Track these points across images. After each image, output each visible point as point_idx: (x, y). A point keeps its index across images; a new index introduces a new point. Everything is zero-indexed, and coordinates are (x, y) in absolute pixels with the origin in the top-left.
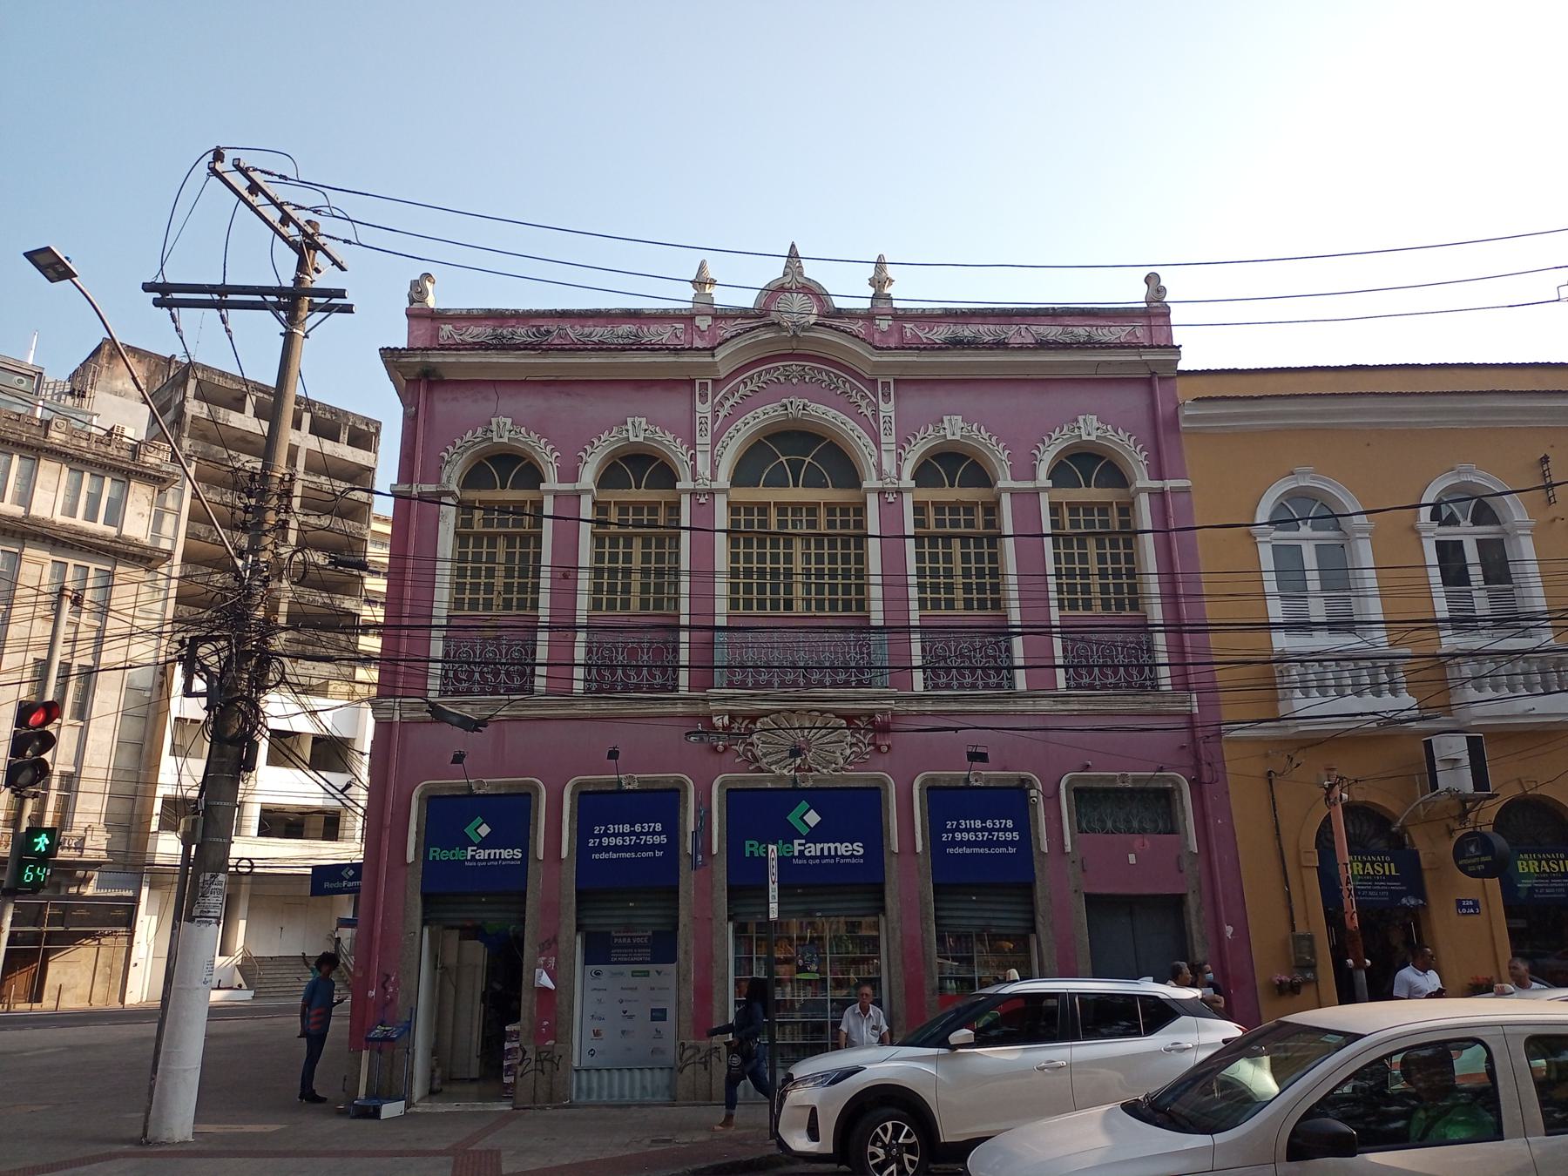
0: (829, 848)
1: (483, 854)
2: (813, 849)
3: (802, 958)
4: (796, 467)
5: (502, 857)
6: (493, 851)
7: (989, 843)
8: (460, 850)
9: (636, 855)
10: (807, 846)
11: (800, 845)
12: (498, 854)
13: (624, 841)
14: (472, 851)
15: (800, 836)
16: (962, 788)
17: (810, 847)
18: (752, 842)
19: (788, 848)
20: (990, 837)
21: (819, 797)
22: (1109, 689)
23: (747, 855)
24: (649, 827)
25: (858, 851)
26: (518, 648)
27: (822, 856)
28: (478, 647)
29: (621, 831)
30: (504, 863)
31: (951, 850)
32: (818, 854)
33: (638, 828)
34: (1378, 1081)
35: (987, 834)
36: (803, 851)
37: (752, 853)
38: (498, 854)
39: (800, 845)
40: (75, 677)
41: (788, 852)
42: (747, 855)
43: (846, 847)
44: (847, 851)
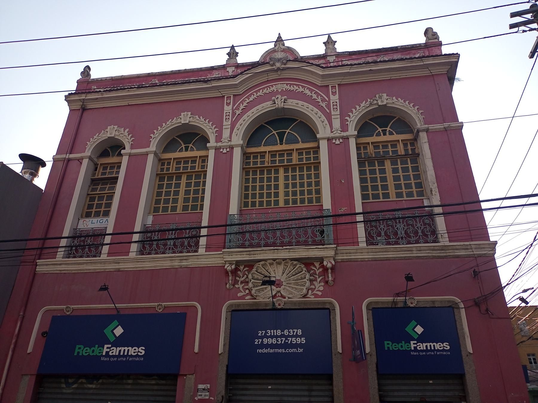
0: (276, 350)
1: (115, 351)
4: (281, 135)
5: (130, 354)
6: (123, 349)
7: (286, 346)
10: (418, 344)
11: (414, 344)
12: (294, 351)
13: (277, 341)
14: (107, 348)
15: (414, 340)
17: (420, 345)
19: (408, 345)
20: (287, 341)
23: (386, 349)
24: (294, 332)
25: (447, 347)
27: (119, 356)
29: (275, 334)
30: (131, 359)
31: (260, 351)
32: (425, 349)
33: (286, 332)
35: (284, 339)
37: (388, 348)
38: (294, 351)
39: (414, 344)
40: (63, 249)
41: (408, 348)
42: (386, 349)
43: (440, 345)
44: (440, 347)
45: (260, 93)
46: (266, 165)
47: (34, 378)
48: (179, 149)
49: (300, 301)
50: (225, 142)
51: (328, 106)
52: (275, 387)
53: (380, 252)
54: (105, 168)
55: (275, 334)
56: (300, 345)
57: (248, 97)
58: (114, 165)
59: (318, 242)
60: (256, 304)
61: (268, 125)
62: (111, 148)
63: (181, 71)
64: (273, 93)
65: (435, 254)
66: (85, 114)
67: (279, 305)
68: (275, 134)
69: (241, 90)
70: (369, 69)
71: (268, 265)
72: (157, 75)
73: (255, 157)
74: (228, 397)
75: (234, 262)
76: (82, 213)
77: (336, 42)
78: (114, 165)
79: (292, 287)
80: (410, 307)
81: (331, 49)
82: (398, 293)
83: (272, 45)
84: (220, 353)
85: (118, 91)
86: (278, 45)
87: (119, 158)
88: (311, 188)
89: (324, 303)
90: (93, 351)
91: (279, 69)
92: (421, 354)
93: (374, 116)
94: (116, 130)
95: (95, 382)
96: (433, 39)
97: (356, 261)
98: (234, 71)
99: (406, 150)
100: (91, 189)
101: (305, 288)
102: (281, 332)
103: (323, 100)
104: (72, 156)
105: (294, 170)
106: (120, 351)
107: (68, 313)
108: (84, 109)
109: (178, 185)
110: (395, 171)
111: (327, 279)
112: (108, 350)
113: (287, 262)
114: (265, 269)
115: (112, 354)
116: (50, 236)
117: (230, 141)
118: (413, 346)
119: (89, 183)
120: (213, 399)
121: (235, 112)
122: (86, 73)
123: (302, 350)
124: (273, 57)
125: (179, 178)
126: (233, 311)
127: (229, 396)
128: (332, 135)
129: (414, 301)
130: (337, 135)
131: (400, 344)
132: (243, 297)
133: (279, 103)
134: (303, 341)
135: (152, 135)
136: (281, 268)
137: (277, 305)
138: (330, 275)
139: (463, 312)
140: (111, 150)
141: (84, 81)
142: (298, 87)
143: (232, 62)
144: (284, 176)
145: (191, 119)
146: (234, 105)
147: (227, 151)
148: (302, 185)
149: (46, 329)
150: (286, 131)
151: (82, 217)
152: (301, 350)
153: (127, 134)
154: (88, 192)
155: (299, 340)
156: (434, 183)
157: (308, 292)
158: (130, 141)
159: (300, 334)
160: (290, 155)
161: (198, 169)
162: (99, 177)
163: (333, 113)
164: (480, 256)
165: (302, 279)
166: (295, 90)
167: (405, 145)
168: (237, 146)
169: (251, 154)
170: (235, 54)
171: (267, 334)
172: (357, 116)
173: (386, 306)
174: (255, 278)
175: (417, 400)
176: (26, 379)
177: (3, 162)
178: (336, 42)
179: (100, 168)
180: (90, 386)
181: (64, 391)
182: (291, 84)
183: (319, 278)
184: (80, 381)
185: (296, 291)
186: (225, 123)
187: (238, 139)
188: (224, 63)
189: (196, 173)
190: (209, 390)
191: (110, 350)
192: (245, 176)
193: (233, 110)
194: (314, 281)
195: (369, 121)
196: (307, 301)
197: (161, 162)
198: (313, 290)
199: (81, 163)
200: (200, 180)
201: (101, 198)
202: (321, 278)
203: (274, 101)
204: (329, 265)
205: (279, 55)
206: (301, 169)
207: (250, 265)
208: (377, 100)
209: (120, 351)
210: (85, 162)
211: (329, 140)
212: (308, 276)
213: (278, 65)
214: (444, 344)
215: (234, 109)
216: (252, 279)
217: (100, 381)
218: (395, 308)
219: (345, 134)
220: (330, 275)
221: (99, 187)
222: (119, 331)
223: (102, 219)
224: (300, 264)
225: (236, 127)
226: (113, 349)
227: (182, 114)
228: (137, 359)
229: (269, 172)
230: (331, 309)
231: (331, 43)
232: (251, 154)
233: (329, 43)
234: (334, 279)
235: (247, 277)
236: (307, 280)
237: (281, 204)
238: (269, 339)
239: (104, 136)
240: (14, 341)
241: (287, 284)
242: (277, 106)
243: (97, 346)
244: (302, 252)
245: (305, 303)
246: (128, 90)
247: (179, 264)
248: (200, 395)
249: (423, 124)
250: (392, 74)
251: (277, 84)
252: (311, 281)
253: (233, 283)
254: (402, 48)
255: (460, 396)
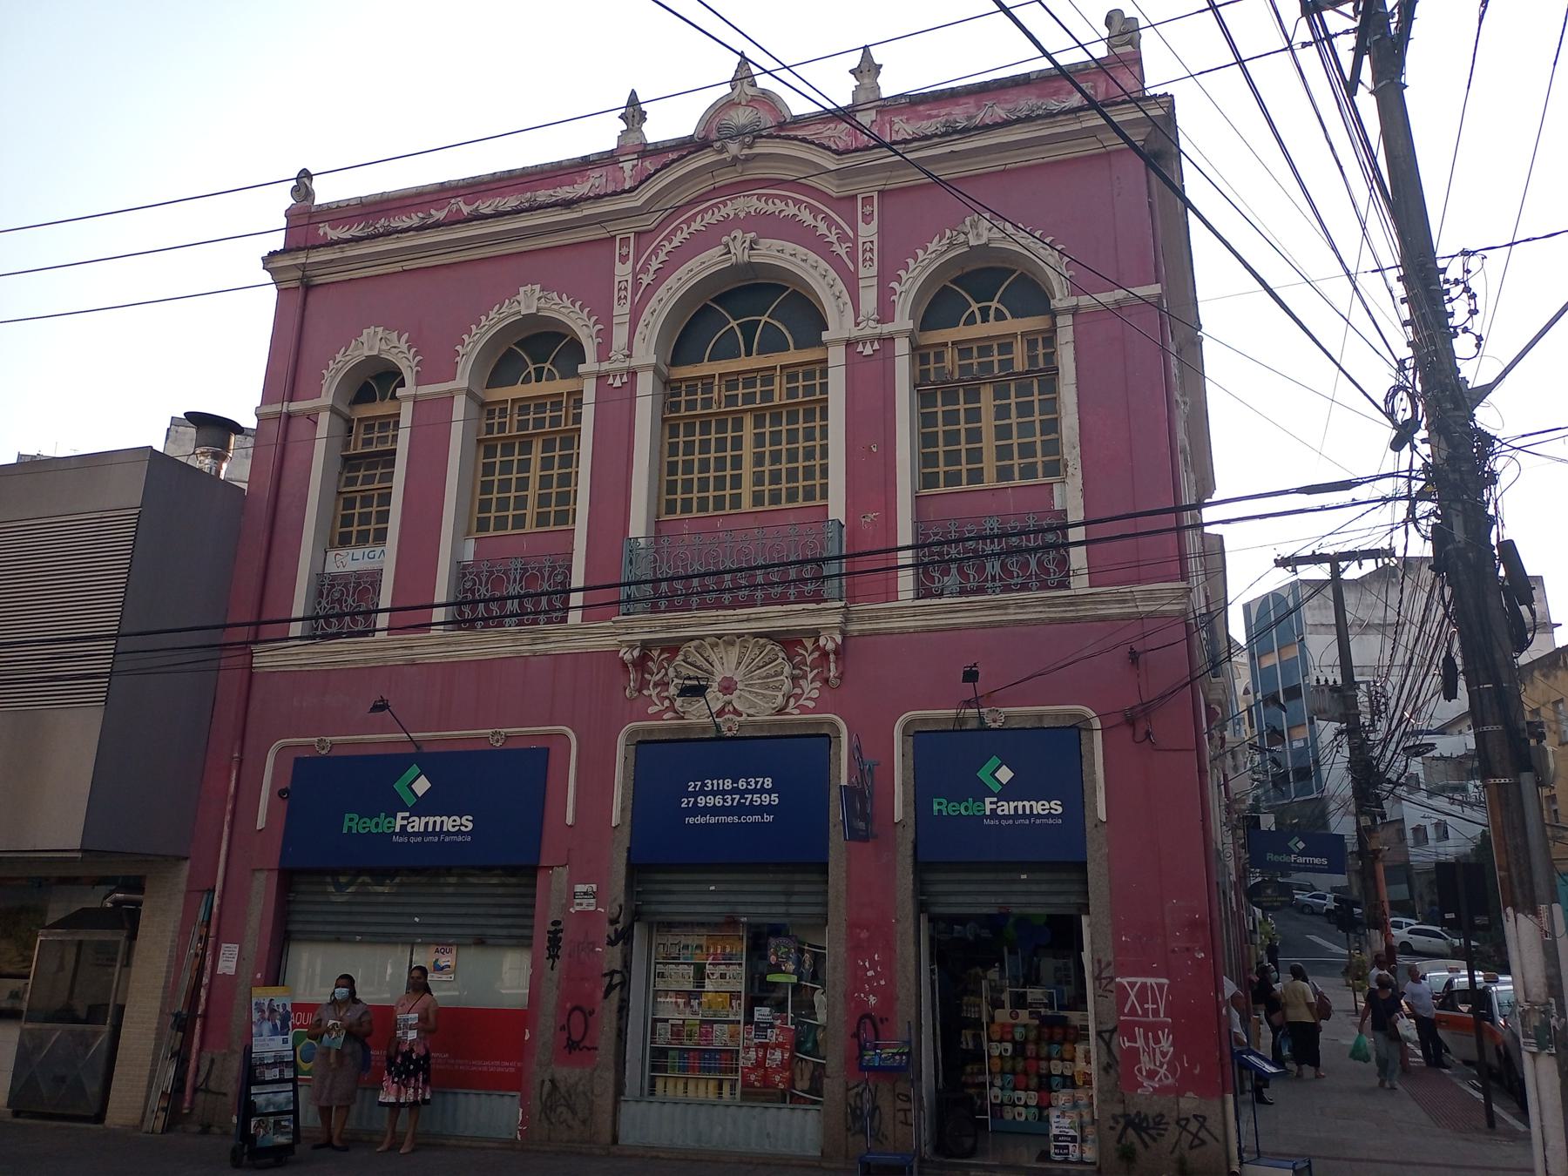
1: (418, 824)
2: (1006, 807)
3: (776, 954)
5: (445, 829)
6: (432, 819)
7: (740, 810)
8: (974, 802)
9: (739, 819)
10: (999, 804)
11: (991, 803)
13: (725, 800)
14: (403, 818)
15: (992, 794)
16: (950, 731)
17: (1003, 806)
18: (351, 816)
19: (390, 822)
20: (742, 801)
21: (429, 762)
22: (1012, 591)
23: (936, 813)
24: (756, 783)
25: (1056, 810)
26: (562, 570)
27: (426, 833)
28: (485, 573)
29: (721, 788)
31: (691, 820)
32: (1012, 812)
33: (742, 784)
34: (236, 1113)
35: (738, 797)
36: (996, 809)
39: (991, 803)
41: (979, 811)
42: (936, 813)
43: (1043, 805)
44: (1043, 810)
45: (695, 226)
46: (714, 409)
47: (275, 877)
48: (522, 377)
49: (771, 721)
50: (617, 363)
51: (852, 254)
52: (723, 887)
53: (940, 613)
54: (369, 429)
55: (721, 788)
56: (769, 809)
57: (668, 238)
58: (388, 420)
59: (809, 597)
60: (685, 728)
61: (717, 304)
62: (377, 377)
63: (515, 173)
64: (726, 225)
65: (1055, 613)
66: (311, 299)
67: (730, 730)
68: (736, 327)
69: (651, 221)
70: (948, 149)
71: (708, 647)
72: (463, 187)
73: (691, 390)
74: (633, 907)
75: (639, 644)
76: (331, 535)
77: (881, 66)
78: (388, 420)
79: (756, 693)
80: (990, 729)
81: (866, 89)
82: (969, 701)
83: (727, 89)
84: (613, 825)
85: (376, 240)
86: (739, 87)
87: (395, 403)
88: (812, 463)
89: (820, 723)
90: (377, 825)
91: (735, 158)
92: (1004, 822)
93: (965, 271)
94: (381, 339)
95: (388, 881)
96: (1121, 45)
97: (889, 633)
98: (637, 165)
99: (1033, 359)
100: (344, 479)
101: (780, 694)
102: (732, 784)
103: (842, 238)
104: (295, 406)
105: (776, 420)
106: (427, 823)
107: (323, 752)
108: (308, 287)
109: (525, 466)
110: (1002, 412)
111: (825, 675)
112: (405, 822)
113: (746, 641)
114: (702, 656)
115: (412, 830)
116: (265, 617)
117: (629, 356)
118: (988, 807)
119: (338, 467)
120: (603, 911)
121: (640, 279)
122: (303, 190)
123: (772, 817)
124: (726, 122)
125: (526, 447)
126: (639, 742)
127: (637, 905)
128: (855, 333)
129: (995, 717)
130: (868, 331)
131: (965, 804)
132: (658, 716)
133: (739, 253)
134: (774, 801)
135: (458, 348)
136: (734, 653)
137: (724, 729)
138: (832, 666)
139: (1098, 736)
140: (377, 384)
141: (302, 211)
142: (784, 203)
143: (631, 141)
144: (755, 434)
145: (542, 303)
146: (636, 262)
147: (622, 383)
148: (792, 456)
149: (286, 784)
150: (760, 318)
151: (332, 546)
152: (769, 818)
153: (404, 347)
154: (338, 488)
155: (766, 799)
156: (1074, 448)
157: (788, 701)
158: (413, 364)
159: (770, 786)
160: (768, 381)
161: (565, 426)
162: (359, 451)
163: (862, 272)
164: (1150, 615)
165: (776, 675)
166: (777, 213)
167: (1032, 344)
168: (645, 367)
169: (681, 382)
170: (637, 118)
171: (706, 788)
172: (915, 279)
173: (943, 727)
174: (683, 674)
175: (994, 911)
176: (261, 877)
177: (152, 447)
178: (881, 66)
179: (358, 426)
180: (380, 889)
181: (333, 899)
182: (768, 196)
183: (811, 671)
184: (360, 880)
185: (763, 702)
186: (617, 310)
187: (647, 350)
188: (612, 144)
189: (563, 435)
190: (594, 895)
191: (409, 823)
192: (670, 438)
193: (635, 275)
194: (801, 678)
195: (952, 286)
196: (783, 720)
197: (487, 408)
198: (798, 697)
199: (316, 423)
200: (571, 452)
201: (367, 501)
202: (815, 671)
203: (727, 245)
204: (830, 646)
205: (741, 117)
206: (792, 418)
207: (672, 648)
208: (966, 234)
209: (427, 824)
210: (324, 419)
211: (850, 344)
212: (787, 670)
213: (734, 148)
214: (1052, 803)
215: (638, 269)
216: (676, 677)
217: (397, 880)
218: (961, 730)
219: (887, 329)
220: (832, 666)
221: (361, 474)
222: (422, 786)
223: (372, 549)
224: (773, 644)
225: (642, 319)
226: (414, 821)
227: (522, 290)
228: (460, 839)
229: (722, 427)
230: (831, 735)
231: (869, 71)
232: (681, 382)
233: (861, 72)
234: (842, 673)
235: (666, 674)
236: (787, 677)
237: (747, 504)
238: (708, 798)
239: (357, 353)
240: (229, 807)
241: (746, 686)
242: (734, 258)
243: (383, 815)
244: (776, 617)
245: (782, 724)
246: (396, 235)
247: (530, 648)
248: (578, 904)
249: (1066, 294)
250: (1007, 158)
251: (737, 197)
252: (794, 679)
253: (637, 687)
254: (1041, 78)
255: (1078, 903)
